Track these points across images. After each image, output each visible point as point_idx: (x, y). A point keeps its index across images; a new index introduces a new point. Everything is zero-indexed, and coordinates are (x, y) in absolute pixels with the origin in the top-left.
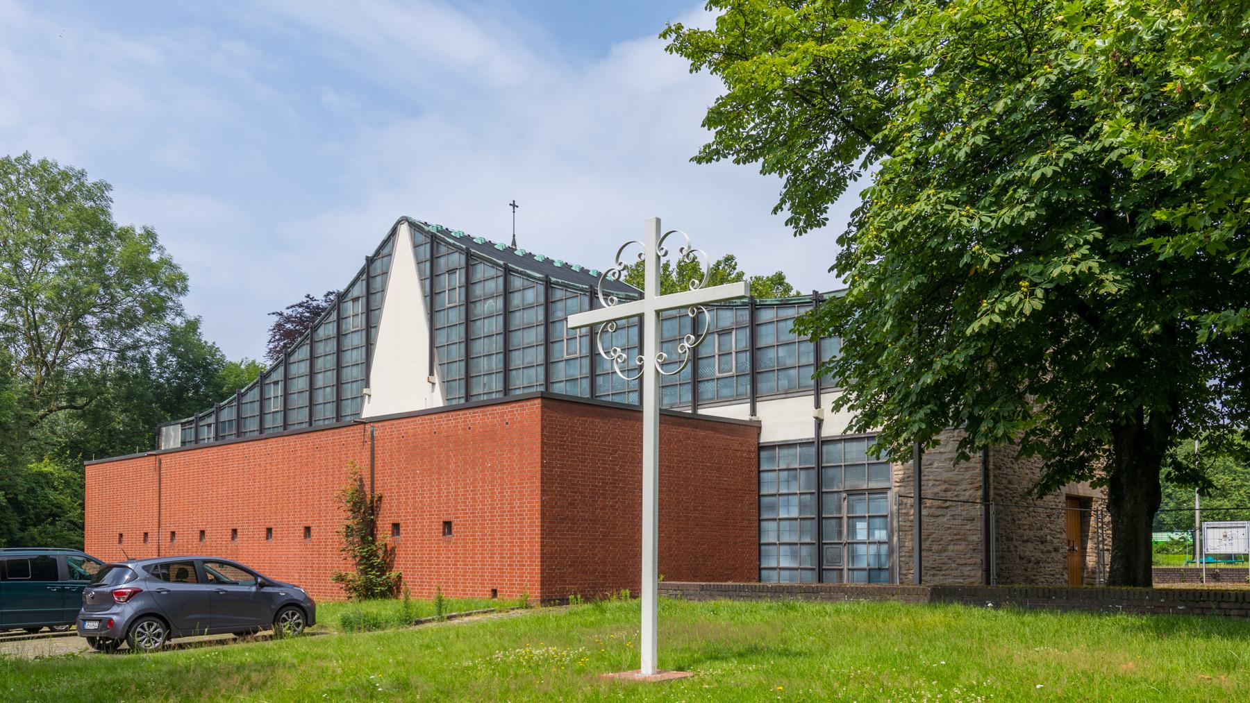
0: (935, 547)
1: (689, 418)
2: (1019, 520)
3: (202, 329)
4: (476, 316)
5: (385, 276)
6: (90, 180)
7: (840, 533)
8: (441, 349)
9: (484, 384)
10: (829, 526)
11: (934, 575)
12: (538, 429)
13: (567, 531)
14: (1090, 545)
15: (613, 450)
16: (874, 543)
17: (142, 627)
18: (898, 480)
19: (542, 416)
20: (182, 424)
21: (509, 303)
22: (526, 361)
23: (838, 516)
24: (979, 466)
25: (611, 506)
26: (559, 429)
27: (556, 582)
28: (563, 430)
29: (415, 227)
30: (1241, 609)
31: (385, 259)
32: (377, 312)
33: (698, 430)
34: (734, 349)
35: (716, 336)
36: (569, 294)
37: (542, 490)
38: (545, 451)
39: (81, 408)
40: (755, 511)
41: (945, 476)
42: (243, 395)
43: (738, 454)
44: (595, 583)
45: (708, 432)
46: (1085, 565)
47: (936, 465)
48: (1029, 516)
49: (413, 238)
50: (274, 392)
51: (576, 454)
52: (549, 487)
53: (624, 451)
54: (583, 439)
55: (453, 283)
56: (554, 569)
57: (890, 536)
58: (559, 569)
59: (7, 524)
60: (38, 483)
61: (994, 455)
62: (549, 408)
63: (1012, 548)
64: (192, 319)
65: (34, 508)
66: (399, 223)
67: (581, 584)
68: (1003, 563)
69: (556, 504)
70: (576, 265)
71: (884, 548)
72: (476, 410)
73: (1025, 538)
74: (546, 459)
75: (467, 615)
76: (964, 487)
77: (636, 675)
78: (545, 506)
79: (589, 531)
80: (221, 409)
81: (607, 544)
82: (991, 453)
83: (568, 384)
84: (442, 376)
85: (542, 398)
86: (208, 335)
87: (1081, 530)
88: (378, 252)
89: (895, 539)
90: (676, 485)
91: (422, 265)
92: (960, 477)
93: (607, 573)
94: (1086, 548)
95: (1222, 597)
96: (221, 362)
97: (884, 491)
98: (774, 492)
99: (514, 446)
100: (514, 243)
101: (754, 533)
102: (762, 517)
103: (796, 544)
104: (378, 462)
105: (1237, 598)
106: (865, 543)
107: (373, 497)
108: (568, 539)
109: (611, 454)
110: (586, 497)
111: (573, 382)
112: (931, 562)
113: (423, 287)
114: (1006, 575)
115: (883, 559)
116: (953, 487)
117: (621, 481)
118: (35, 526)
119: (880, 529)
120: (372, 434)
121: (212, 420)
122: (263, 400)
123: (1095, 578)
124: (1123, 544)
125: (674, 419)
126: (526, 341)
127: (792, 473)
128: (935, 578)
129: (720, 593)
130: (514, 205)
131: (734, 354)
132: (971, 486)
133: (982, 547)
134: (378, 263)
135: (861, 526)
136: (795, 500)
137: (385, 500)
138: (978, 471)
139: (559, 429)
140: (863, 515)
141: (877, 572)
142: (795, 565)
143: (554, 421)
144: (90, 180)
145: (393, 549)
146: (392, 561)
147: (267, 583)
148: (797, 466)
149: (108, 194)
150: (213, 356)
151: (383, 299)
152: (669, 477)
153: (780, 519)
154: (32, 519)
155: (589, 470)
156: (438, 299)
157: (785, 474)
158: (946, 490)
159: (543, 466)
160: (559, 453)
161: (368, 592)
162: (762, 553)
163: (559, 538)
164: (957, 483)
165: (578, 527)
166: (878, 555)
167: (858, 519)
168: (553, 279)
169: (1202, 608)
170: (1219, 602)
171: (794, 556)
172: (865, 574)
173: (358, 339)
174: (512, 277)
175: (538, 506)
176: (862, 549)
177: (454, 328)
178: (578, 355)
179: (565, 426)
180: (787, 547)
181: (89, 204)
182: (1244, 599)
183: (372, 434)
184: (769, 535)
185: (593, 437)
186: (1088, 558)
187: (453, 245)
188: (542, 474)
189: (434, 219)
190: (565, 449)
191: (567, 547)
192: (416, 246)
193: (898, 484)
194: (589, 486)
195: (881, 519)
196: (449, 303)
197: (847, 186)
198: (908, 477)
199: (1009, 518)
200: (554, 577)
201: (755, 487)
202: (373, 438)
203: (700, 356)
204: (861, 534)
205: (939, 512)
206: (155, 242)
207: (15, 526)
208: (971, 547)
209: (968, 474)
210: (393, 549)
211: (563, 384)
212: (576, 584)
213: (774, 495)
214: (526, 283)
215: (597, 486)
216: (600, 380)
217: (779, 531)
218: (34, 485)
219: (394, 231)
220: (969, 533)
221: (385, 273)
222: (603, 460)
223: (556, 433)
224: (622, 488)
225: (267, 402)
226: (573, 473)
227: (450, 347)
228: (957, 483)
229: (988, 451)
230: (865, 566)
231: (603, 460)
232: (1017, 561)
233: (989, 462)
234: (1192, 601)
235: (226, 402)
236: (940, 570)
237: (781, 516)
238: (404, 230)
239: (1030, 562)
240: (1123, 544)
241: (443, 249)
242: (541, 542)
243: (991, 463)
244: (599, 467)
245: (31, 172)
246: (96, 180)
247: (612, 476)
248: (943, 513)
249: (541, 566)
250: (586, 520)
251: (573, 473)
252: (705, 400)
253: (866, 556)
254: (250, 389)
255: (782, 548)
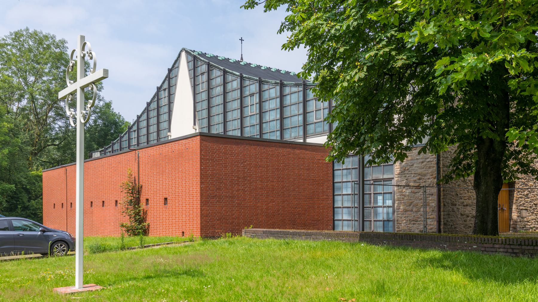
0: (414, 209)
1: (290, 144)
2: (461, 194)
3: (113, 106)
4: (212, 95)
5: (176, 77)
6: (57, 39)
7: (370, 203)
8: (199, 112)
9: (216, 129)
10: (367, 197)
11: (414, 224)
12: (199, 151)
13: (216, 202)
14: (514, 207)
15: (243, 161)
16: (386, 207)
17: (58, 246)
18: (397, 174)
19: (201, 145)
20: (100, 151)
21: (226, 88)
22: (233, 117)
23: (369, 193)
24: (435, 165)
25: (242, 189)
26: (211, 151)
27: (210, 229)
28: (213, 151)
29: (187, 52)
30: (504, 248)
31: (176, 69)
32: (173, 95)
33: (295, 150)
34: (322, 107)
35: (314, 101)
36: (251, 83)
37: (201, 182)
38: (203, 162)
39: (57, 145)
40: (331, 191)
41: (419, 171)
42: (122, 137)
43: (321, 161)
44: (233, 229)
45: (301, 150)
46: (511, 217)
47: (415, 165)
48: (468, 192)
49: (187, 58)
50: (134, 135)
51: (221, 164)
52: (205, 180)
53: (250, 161)
54: (225, 156)
55: (203, 80)
56: (209, 222)
57: (394, 203)
58: (211, 222)
59: (22, 199)
60: (36, 180)
61: (443, 160)
62: (205, 141)
63: (455, 209)
64: (108, 102)
65: (35, 192)
66: (181, 51)
67: (224, 229)
68: (449, 218)
69: (209, 189)
70: (274, 68)
71: (391, 210)
72: (176, 142)
73: (465, 204)
74: (203, 166)
75: (157, 245)
76: (428, 177)
77: (74, 289)
78: (203, 190)
79: (229, 203)
80: (114, 144)
81: (240, 208)
82: (441, 159)
83: (251, 127)
84: (199, 126)
85: (200, 135)
86: (116, 108)
87: (510, 199)
88: (173, 66)
89: (396, 205)
90: (282, 178)
91: (191, 71)
92: (426, 172)
93: (240, 223)
94: (512, 209)
95: (495, 241)
96: (123, 122)
97: (390, 179)
98: (340, 181)
99: (190, 160)
100: (242, 59)
101: (330, 202)
102: (336, 193)
103: (350, 207)
104: (141, 169)
105: (502, 242)
106: (381, 207)
107: (139, 186)
108: (217, 206)
109: (242, 163)
110: (228, 185)
111: (253, 127)
112: (412, 217)
113: (191, 82)
114: (451, 224)
115: (391, 215)
116: (423, 177)
117: (248, 176)
118: (34, 200)
119: (388, 199)
120: (138, 155)
121: (110, 149)
122: (129, 139)
123: (516, 225)
124: (480, 209)
125: (280, 144)
126: (233, 107)
127: (349, 170)
128: (414, 225)
129: (271, 235)
130: (242, 40)
131: (322, 110)
132: (431, 177)
133: (436, 209)
134: (173, 72)
135: (380, 198)
136: (349, 185)
137: (143, 188)
138: (435, 168)
139: (211, 151)
140: (381, 192)
141: (387, 222)
142: (350, 219)
143: (208, 147)
144: (57, 39)
145: (146, 211)
146: (146, 217)
147: (46, 230)
148: (350, 167)
149: (66, 45)
150: (119, 118)
151: (176, 88)
152: (277, 174)
153: (343, 195)
154: (34, 197)
155: (229, 172)
156: (197, 87)
157: (345, 171)
158: (419, 179)
159: (201, 170)
160: (211, 163)
161: (133, 232)
162: (335, 212)
163: (211, 206)
164: (425, 175)
165: (223, 200)
166: (388, 213)
167: (379, 195)
168: (244, 75)
169: (485, 247)
170: (493, 244)
171: (349, 213)
172: (382, 223)
173: (165, 109)
174: (227, 75)
175: (199, 190)
176: (380, 210)
177: (204, 102)
178: (255, 113)
179: (215, 149)
180: (346, 209)
181: (58, 50)
182: (506, 242)
183: (138, 155)
184: (338, 204)
185: (231, 155)
186: (513, 214)
187: (203, 61)
188: (201, 174)
189: (198, 48)
190: (215, 161)
191: (216, 211)
192: (188, 62)
193: (397, 176)
194: (229, 179)
195: (389, 195)
196: (202, 89)
197: (247, 9)
198: (402, 172)
199: (454, 194)
200: (208, 226)
201: (331, 178)
202: (138, 157)
203: (307, 112)
204: (380, 203)
205: (416, 190)
206: (89, 66)
207: (25, 200)
208: (431, 209)
209: (430, 170)
210: (146, 211)
211: (249, 128)
212: (222, 229)
213: (340, 182)
214: (233, 78)
215: (234, 180)
216: (264, 125)
217: (343, 201)
218: (34, 181)
219: (179, 55)
220: (431, 201)
221: (176, 76)
222: (237, 166)
223: (209, 153)
224: (249, 180)
225: (131, 140)
226: (219, 173)
227: (203, 111)
228: (425, 175)
229: (440, 158)
230: (381, 219)
231: (237, 166)
232: (459, 216)
233: (440, 164)
234: (480, 243)
235: (116, 140)
236: (417, 221)
237: (344, 193)
238: (183, 54)
239: (468, 216)
240: (480, 209)
241: (199, 63)
242: (201, 208)
243: (441, 164)
244: (235, 170)
245: (31, 36)
246: (61, 39)
247: (243, 174)
248: (418, 191)
249: (201, 220)
250: (227, 197)
251: (219, 173)
252: (309, 134)
253: (382, 214)
254: (125, 134)
255: (344, 209)
